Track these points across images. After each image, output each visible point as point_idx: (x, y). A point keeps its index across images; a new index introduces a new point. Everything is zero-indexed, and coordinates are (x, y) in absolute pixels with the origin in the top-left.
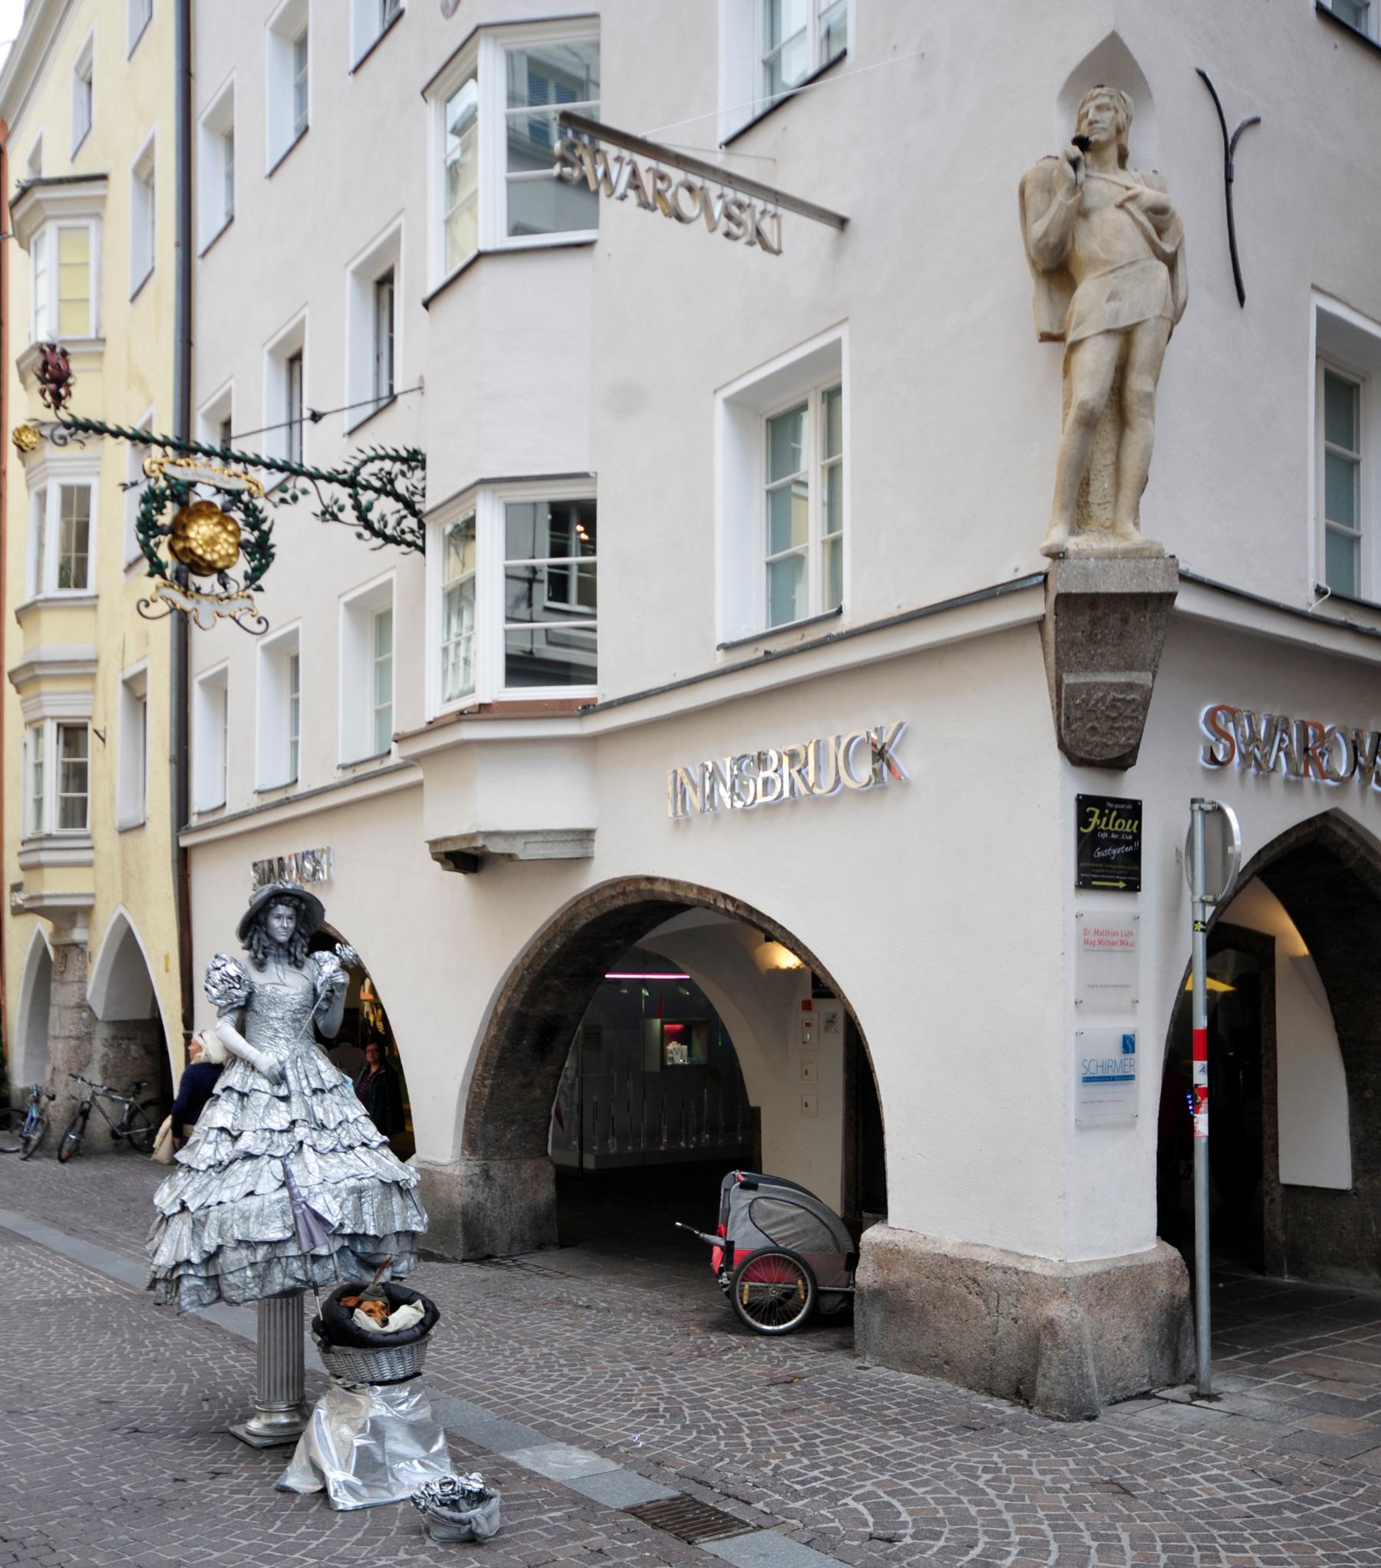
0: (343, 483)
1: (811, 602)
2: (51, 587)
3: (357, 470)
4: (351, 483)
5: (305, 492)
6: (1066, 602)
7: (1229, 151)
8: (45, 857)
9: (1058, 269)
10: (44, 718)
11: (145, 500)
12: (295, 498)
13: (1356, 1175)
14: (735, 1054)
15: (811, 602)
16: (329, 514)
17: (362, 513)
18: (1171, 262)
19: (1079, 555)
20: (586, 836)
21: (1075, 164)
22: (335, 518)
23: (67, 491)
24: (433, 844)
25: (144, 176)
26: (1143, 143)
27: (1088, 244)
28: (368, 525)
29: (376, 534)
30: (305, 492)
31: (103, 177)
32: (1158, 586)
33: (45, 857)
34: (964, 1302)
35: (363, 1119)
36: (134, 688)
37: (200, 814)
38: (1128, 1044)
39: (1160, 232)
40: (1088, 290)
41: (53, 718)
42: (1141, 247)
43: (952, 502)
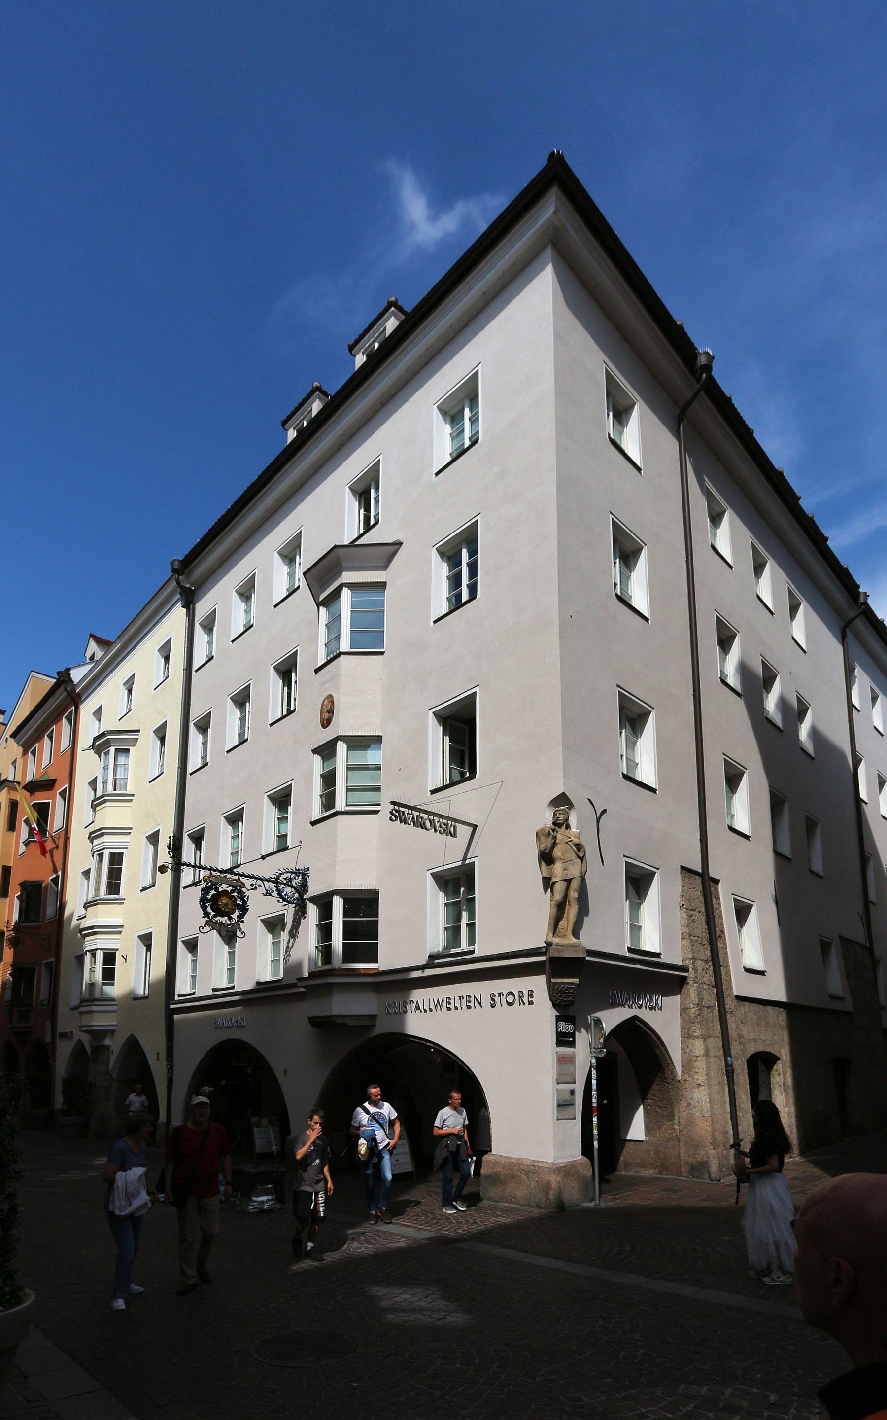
0: (273, 882)
1: (464, 946)
2: (103, 893)
3: (278, 877)
4: (276, 881)
5: (260, 886)
6: (551, 959)
7: (598, 822)
8: (94, 1008)
9: (546, 858)
10: (97, 949)
11: (203, 890)
12: (256, 888)
13: (646, 1136)
14: (282, 1095)
15: (464, 946)
16: (268, 894)
17: (280, 892)
18: (582, 859)
19: (557, 945)
20: (373, 1017)
21: (554, 830)
22: (270, 895)
23: (112, 854)
24: (310, 1018)
25: (161, 733)
26: (573, 820)
27: (557, 852)
28: (281, 897)
29: (284, 900)
30: (260, 886)
31: (138, 731)
32: (581, 955)
33: (94, 1008)
34: (520, 1178)
35: (776, 1086)
36: (146, 940)
37: (180, 996)
38: (572, 1092)
39: (579, 850)
40: (558, 867)
41: (101, 949)
42: (574, 856)
43: (513, 915)
